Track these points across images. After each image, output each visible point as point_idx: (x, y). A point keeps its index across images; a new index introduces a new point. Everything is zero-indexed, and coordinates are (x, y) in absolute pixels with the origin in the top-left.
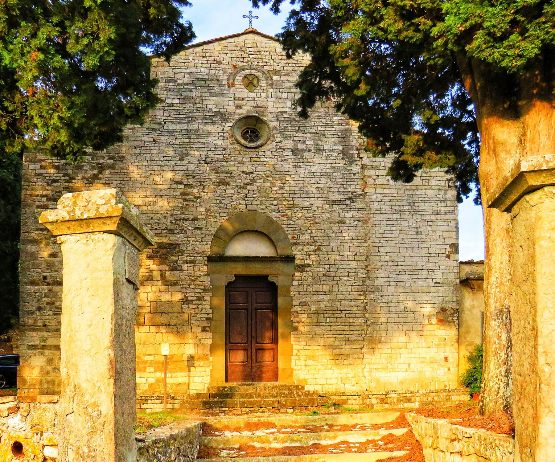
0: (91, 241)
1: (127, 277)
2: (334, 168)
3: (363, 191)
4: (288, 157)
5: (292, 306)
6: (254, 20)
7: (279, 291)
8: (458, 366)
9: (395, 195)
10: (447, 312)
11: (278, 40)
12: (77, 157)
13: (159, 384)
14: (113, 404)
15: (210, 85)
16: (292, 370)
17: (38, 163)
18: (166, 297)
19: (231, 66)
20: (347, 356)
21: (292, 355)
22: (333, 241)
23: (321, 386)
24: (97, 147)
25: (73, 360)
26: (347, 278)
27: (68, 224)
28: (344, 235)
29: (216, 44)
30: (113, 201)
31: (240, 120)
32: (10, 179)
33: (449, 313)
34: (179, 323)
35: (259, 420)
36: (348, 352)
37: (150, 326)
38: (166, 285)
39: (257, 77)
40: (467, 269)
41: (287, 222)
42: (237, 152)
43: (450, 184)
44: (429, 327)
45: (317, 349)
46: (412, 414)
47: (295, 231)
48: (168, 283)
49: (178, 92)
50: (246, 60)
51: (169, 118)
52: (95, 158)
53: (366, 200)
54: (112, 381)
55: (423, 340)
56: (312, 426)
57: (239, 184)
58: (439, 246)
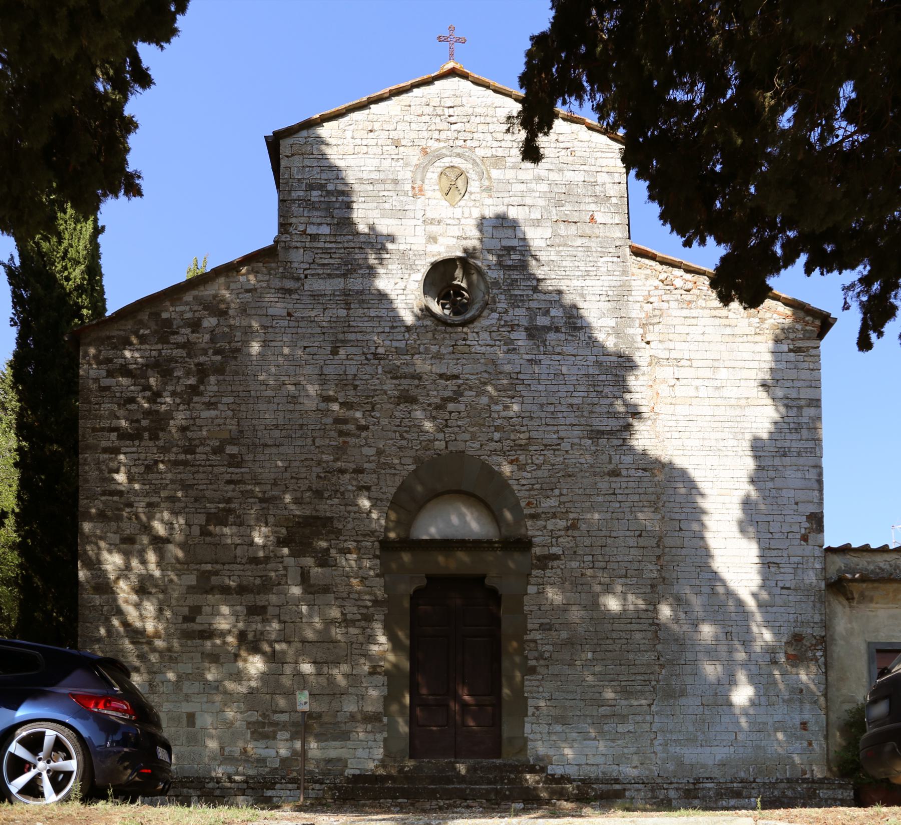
4: (520, 343)
9: (708, 418)
10: (804, 642)
15: (381, 194)
16: (526, 740)
19: (417, 150)
21: (526, 715)
23: (577, 767)
33: (808, 644)
40: (839, 562)
42: (430, 335)
47: (532, 492)
49: (327, 209)
50: (443, 135)
51: (312, 266)
53: (658, 429)
58: (788, 519)
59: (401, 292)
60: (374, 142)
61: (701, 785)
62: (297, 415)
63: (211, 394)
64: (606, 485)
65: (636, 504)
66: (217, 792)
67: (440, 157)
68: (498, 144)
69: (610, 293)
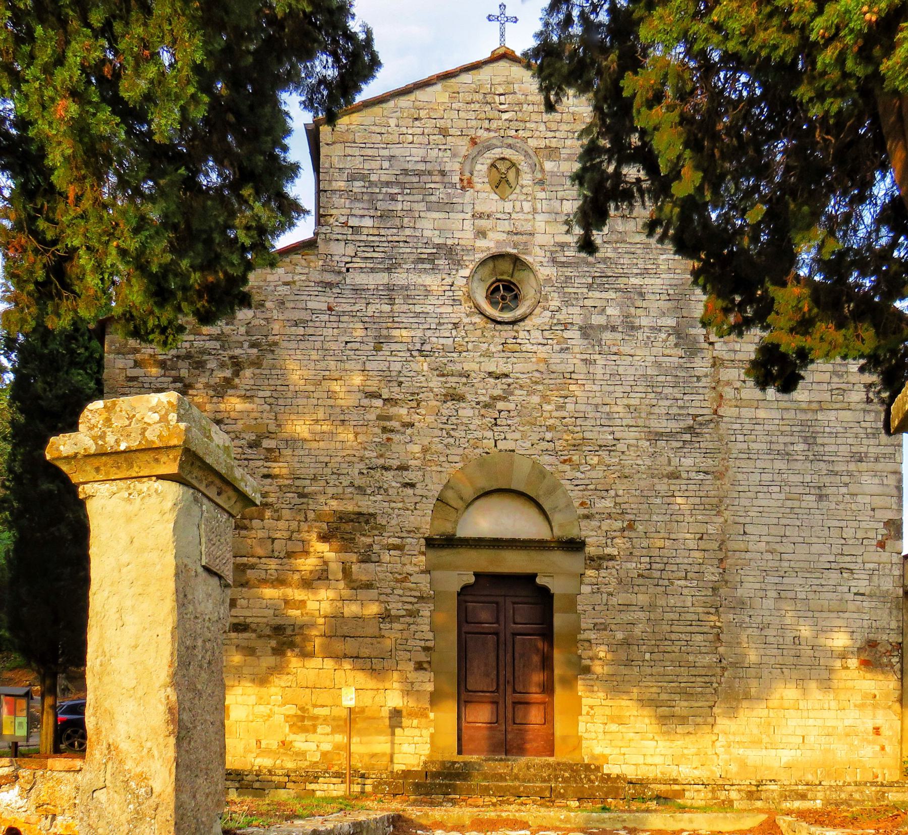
0: (135, 494)
1: (204, 564)
2: (659, 365)
3: (715, 412)
4: (573, 342)
5: (578, 630)
6: (509, 26)
7: (556, 604)
8: (901, 742)
9: (777, 422)
10: (879, 648)
11: (528, 66)
12: (167, 337)
13: (339, 754)
14: (173, 777)
15: (428, 186)
16: (580, 739)
17: (131, 356)
18: (352, 609)
20: (684, 720)
21: (581, 715)
22: (657, 511)
23: (634, 767)
24: (206, 318)
26: (682, 583)
27: (96, 462)
28: (679, 500)
29: (438, 87)
30: (173, 417)
31: (483, 263)
32: (90, 389)
33: (883, 650)
34: (374, 654)
35: (499, 816)
36: (685, 712)
37: (323, 658)
38: (353, 588)
39: (514, 165)
41: (570, 474)
42: (479, 332)
43: (871, 395)
44: (843, 674)
45: (627, 706)
46: (788, 818)
47: (585, 493)
48: (355, 585)
49: (371, 201)
50: (494, 125)
51: (354, 260)
52: (226, 346)
53: (721, 432)
54: (172, 741)
55: (832, 697)
56: (598, 829)
57: (482, 398)
58: (863, 525)
59: (448, 288)
60: (419, 131)
61: (764, 787)
62: (338, 410)
63: (248, 387)
64: (665, 487)
65: (696, 507)
66: (257, 785)
67: (489, 148)
68: (552, 134)
69: (671, 292)
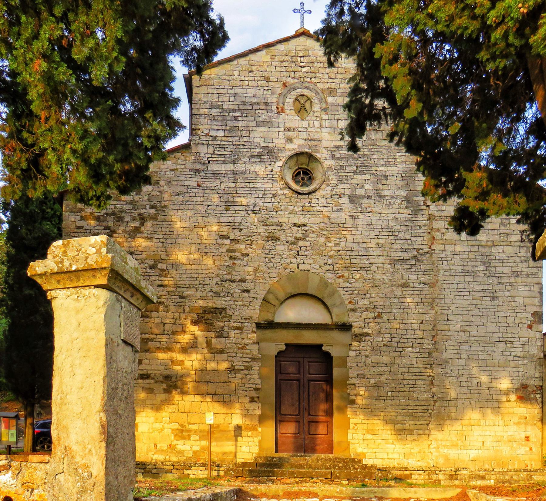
0: (81, 296)
1: (122, 338)
2: (396, 219)
3: (430, 247)
5: (348, 378)
6: (306, 15)
7: (335, 362)
8: (542, 445)
9: (467, 253)
10: (529, 389)
11: (318, 40)
12: (100, 202)
13: (204, 452)
14: (104, 466)
15: (257, 112)
16: (349, 444)
17: (79, 214)
18: (212, 365)
20: (411, 432)
21: (349, 429)
22: (395, 307)
23: (381, 460)
24: (124, 191)
25: (64, 423)
26: (410, 350)
27: (58, 277)
28: (408, 300)
29: (264, 52)
30: (104, 250)
31: (291, 158)
32: (54, 233)
34: (225, 392)
35: (300, 490)
36: (412, 427)
37: (194, 395)
38: (212, 353)
41: (343, 285)
42: (288, 199)
43: (524, 237)
44: (507, 404)
45: (377, 424)
46: (474, 491)
47: (352, 296)
48: (214, 351)
49: (223, 121)
50: (297, 75)
51: (213, 156)
52: (136, 207)
53: (433, 259)
54: (103, 444)
56: (360, 497)
58: (519, 315)
64: (400, 292)
